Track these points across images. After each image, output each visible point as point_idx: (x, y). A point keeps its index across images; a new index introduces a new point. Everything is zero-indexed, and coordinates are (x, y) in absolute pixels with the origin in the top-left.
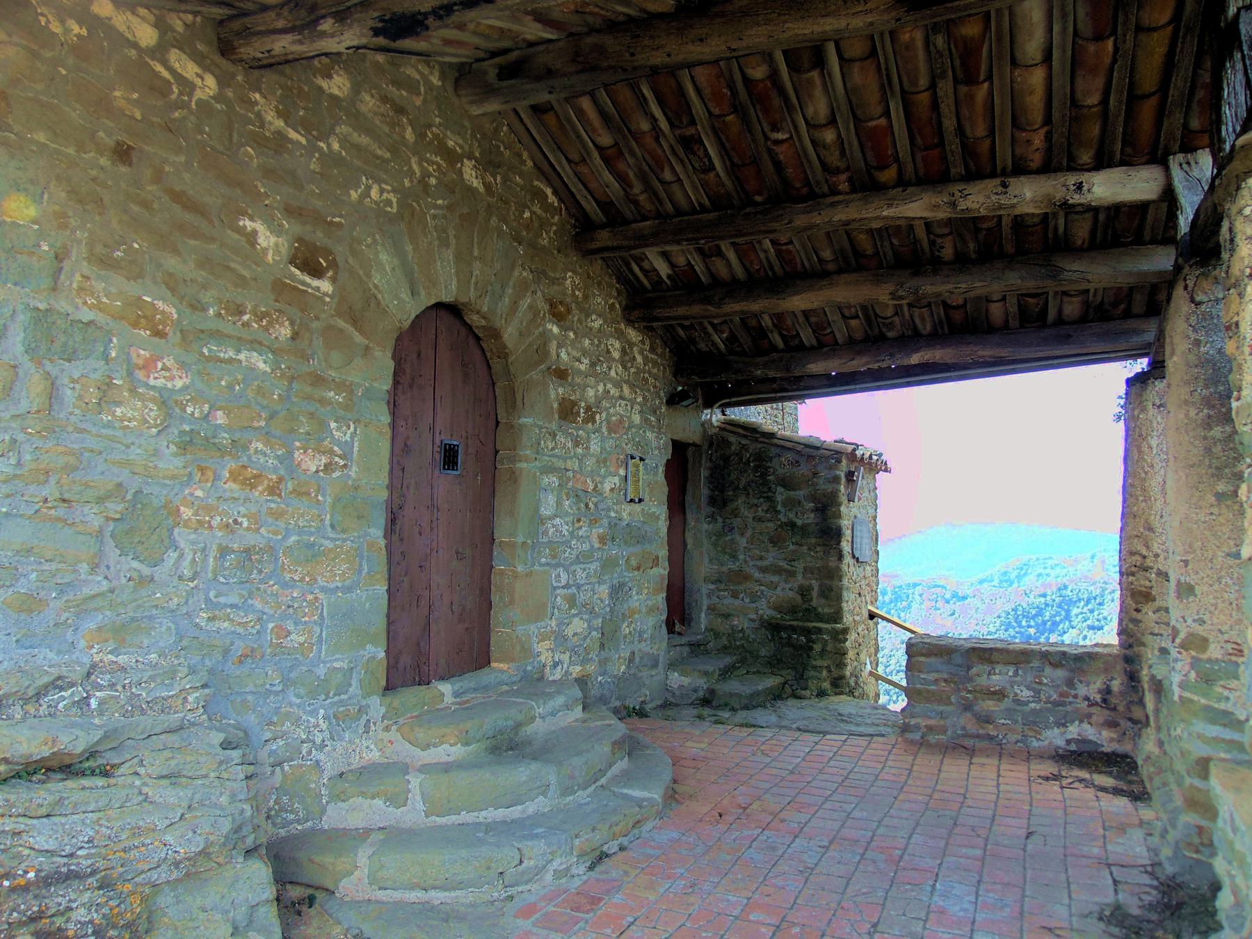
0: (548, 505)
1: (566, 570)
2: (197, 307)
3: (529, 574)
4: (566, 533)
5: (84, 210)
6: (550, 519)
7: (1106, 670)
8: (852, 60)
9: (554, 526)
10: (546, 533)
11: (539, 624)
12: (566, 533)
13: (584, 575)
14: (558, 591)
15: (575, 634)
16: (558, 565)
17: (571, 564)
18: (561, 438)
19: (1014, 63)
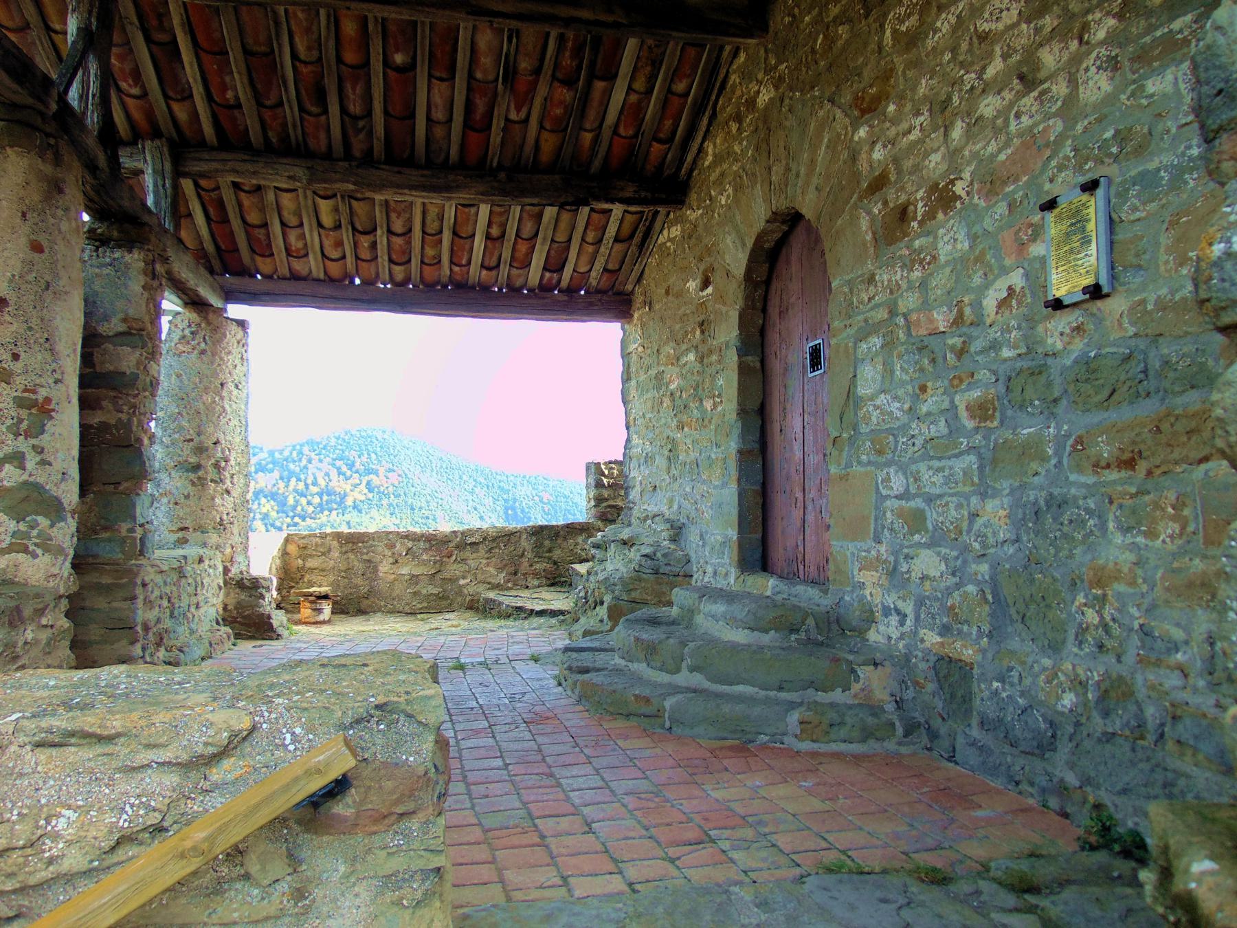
0: (869, 377)
1: (903, 468)
2: (320, 611)
3: (844, 478)
4: (899, 414)
5: (61, 597)
6: (872, 400)
7: (987, 84)
8: (635, 91)
9: (876, 407)
10: (867, 419)
11: (859, 545)
12: (899, 414)
13: (938, 479)
14: (888, 503)
15: (924, 578)
16: (888, 464)
17: (913, 461)
18: (883, 277)
19: (24, 585)
